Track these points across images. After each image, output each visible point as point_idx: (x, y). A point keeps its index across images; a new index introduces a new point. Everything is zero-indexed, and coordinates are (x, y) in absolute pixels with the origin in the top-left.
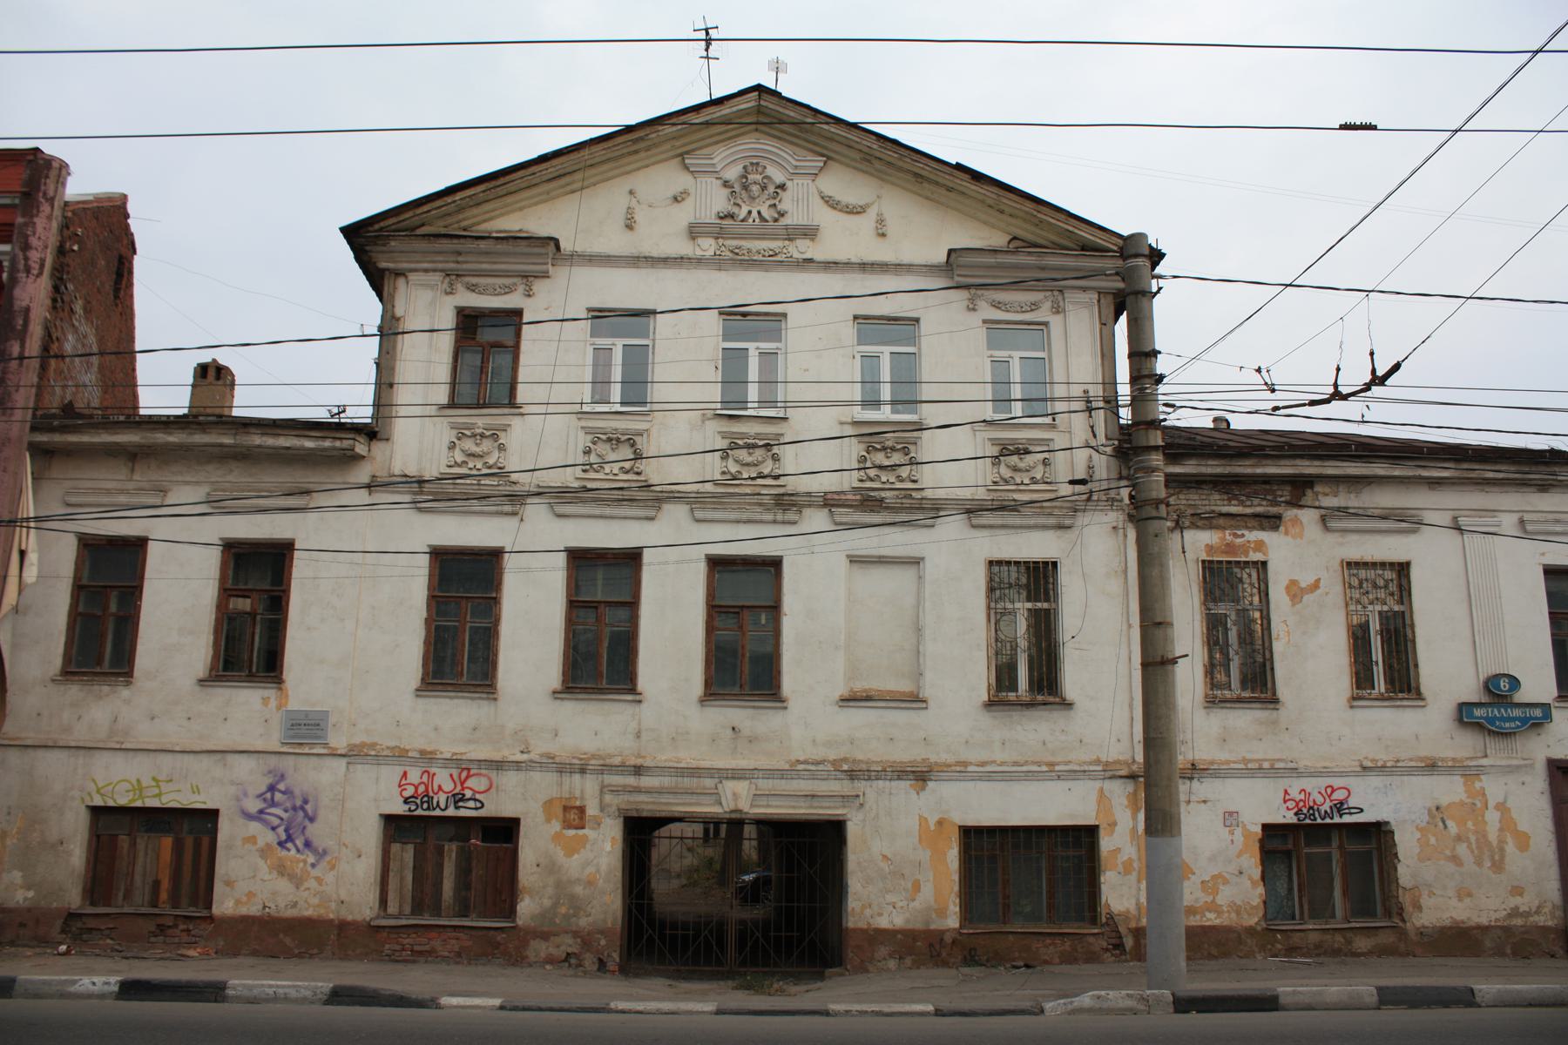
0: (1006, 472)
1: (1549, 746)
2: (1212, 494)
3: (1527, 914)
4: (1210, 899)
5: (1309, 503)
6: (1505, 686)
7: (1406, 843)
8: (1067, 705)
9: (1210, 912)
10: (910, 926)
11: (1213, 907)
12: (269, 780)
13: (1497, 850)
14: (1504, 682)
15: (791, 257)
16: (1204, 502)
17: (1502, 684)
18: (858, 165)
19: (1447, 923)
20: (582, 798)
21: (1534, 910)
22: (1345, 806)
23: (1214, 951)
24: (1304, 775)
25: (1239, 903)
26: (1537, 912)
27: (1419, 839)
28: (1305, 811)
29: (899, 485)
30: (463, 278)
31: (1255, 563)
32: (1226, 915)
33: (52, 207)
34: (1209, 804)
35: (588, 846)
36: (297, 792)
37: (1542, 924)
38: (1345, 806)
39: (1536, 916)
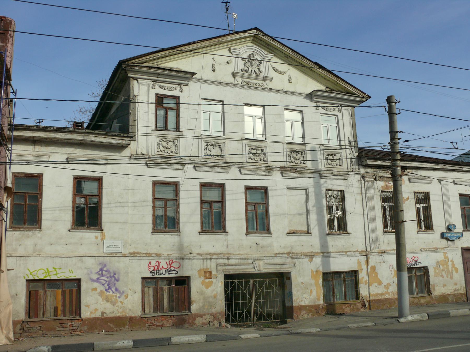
3: (458, 290)
4: (386, 290)
10: (310, 304)
11: (387, 293)
12: (100, 267)
18: (283, 59)
19: (441, 294)
20: (211, 268)
21: (459, 289)
26: (460, 290)
28: (408, 264)
34: (385, 263)
35: (213, 285)
36: (111, 271)
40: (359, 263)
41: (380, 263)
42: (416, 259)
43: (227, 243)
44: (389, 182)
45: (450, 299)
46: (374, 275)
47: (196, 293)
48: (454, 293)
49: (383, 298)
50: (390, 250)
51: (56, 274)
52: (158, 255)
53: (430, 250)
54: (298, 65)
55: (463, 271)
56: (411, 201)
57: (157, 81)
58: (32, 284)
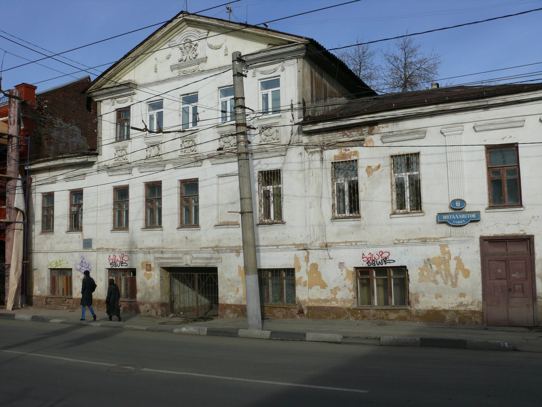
0: (263, 136)
1: (482, 230)
2: (336, 134)
3: (466, 305)
4: (333, 296)
5: (376, 132)
6: (458, 205)
7: (413, 274)
8: (283, 223)
9: (334, 301)
10: (236, 303)
11: (335, 299)
12: (81, 260)
13: (454, 278)
14: (458, 202)
15: (199, 71)
16: (333, 138)
17: (457, 204)
18: (217, 30)
19: (430, 308)
20: (150, 262)
21: (470, 303)
22: (388, 260)
23: (335, 317)
24: (370, 247)
25: (344, 298)
26: (471, 304)
27: (419, 273)
28: (371, 262)
29: (273, 141)
30: (116, 99)
31: (353, 161)
32: (340, 302)
33: (15, 104)
34: (333, 259)
35: (152, 277)
36: (87, 263)
37: (473, 310)
38: (388, 260)
39: (471, 306)
40: (296, 259)
41: (325, 259)
42: (385, 255)
43: (163, 237)
44: (347, 149)
45: (448, 318)
46: (315, 275)
47: (140, 284)
48: (456, 309)
49: (328, 306)
50: (339, 243)
51: (60, 265)
52: (113, 250)
53: (410, 241)
54: (230, 31)
55: (481, 275)
56: (383, 170)
57: (115, 98)
58: (53, 271)
